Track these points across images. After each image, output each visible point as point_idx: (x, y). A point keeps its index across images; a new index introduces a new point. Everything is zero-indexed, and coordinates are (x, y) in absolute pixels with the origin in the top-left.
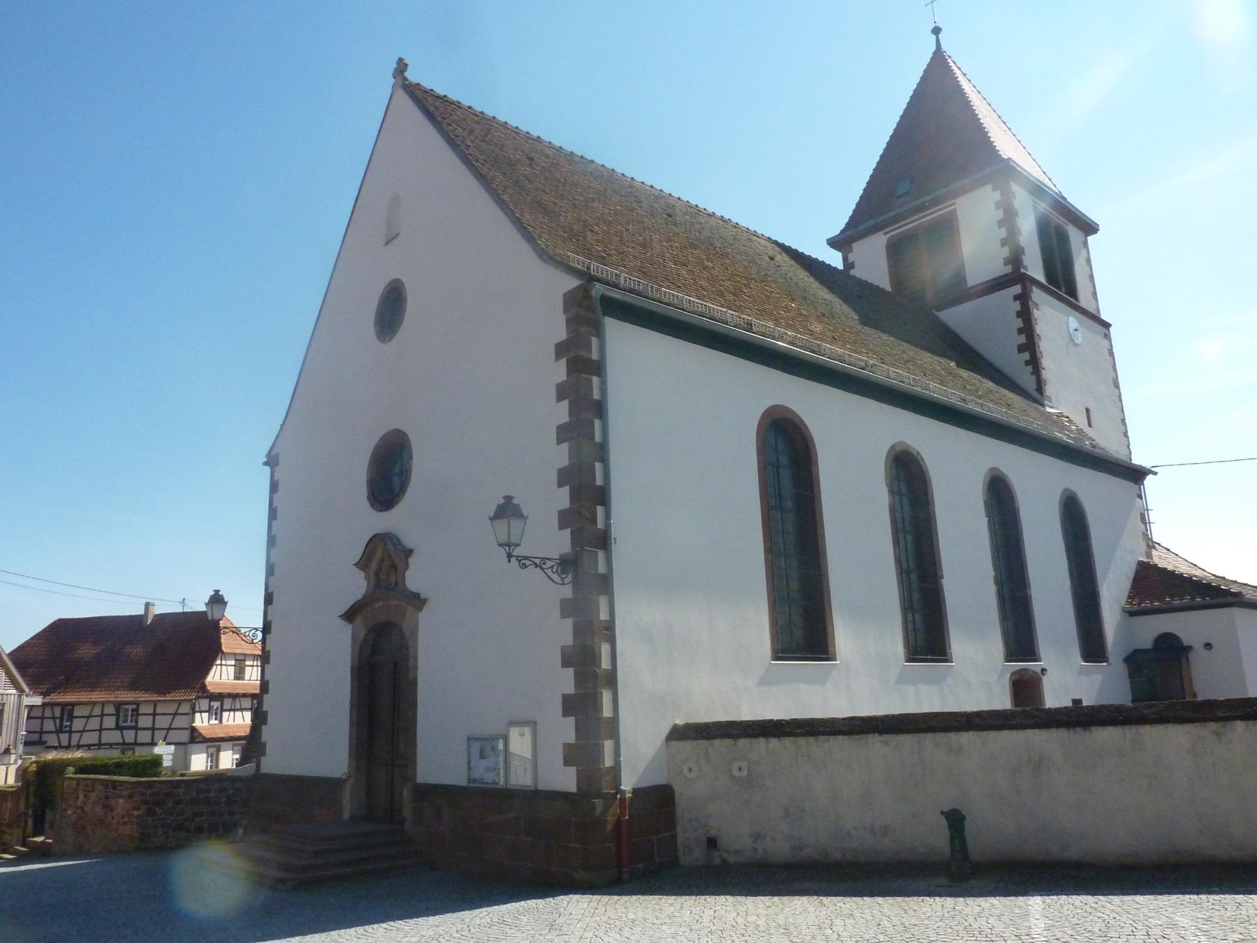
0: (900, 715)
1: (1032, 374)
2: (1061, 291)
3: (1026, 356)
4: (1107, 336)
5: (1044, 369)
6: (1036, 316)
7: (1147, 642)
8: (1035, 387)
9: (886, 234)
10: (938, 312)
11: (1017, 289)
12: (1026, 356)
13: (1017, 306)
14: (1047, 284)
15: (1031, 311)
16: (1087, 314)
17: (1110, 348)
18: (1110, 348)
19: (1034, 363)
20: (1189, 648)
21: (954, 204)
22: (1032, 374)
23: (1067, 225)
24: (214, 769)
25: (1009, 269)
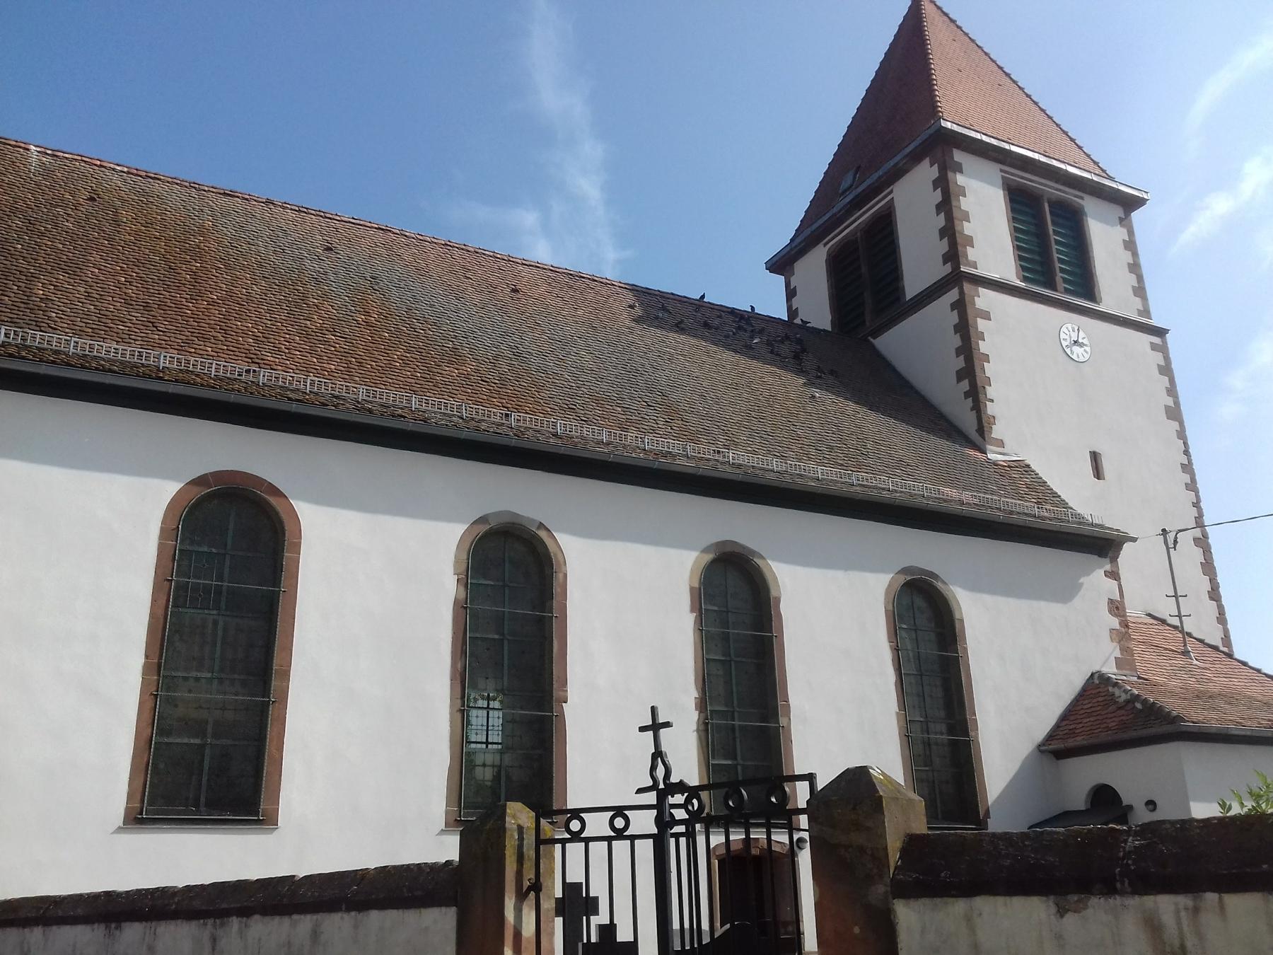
0: (384, 869)
1: (972, 409)
2: (1054, 288)
3: (965, 385)
4: (1163, 349)
5: (992, 401)
6: (980, 329)
7: (1078, 799)
8: (976, 428)
9: (825, 245)
10: (874, 339)
11: (953, 295)
12: (965, 385)
13: (954, 317)
14: (1022, 285)
15: (970, 322)
16: (1143, 328)
17: (1162, 363)
18: (1162, 363)
19: (976, 395)
20: (1130, 807)
21: (891, 192)
22: (972, 409)
23: (1082, 198)
24: (206, 921)
25: (948, 268)
